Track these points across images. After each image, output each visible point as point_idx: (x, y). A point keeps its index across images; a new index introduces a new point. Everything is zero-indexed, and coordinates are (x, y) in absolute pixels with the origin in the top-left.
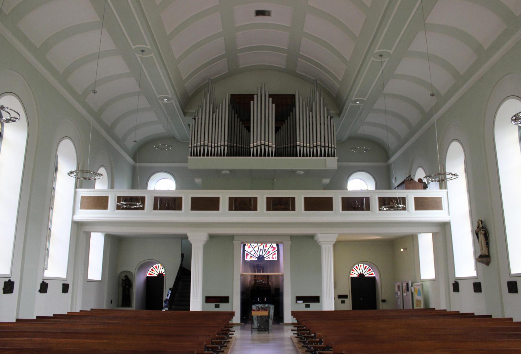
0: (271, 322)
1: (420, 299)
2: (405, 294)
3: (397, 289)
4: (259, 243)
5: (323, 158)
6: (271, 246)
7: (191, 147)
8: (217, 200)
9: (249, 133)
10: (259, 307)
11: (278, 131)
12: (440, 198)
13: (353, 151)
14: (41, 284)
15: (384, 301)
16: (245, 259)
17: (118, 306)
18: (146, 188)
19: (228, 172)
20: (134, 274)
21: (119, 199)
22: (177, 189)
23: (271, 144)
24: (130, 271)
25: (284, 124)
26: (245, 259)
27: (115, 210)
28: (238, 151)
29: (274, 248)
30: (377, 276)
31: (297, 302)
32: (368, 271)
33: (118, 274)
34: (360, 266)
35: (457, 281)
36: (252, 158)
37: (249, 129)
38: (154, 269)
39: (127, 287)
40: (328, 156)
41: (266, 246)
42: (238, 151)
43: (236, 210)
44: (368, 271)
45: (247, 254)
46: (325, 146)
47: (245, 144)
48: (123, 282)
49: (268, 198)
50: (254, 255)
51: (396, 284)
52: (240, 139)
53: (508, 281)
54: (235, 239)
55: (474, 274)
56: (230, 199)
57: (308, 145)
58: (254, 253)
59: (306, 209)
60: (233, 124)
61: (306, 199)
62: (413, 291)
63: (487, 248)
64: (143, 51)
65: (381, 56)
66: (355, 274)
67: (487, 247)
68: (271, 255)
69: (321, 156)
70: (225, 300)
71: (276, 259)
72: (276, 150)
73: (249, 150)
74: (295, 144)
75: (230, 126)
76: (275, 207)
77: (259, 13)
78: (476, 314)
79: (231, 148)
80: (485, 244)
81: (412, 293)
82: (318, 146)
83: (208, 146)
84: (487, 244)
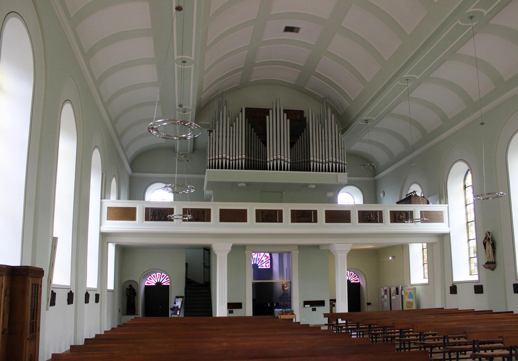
1: (412, 301)
2: (393, 298)
3: (383, 293)
5: (334, 173)
6: (265, 255)
7: (210, 160)
8: (244, 212)
9: (265, 147)
10: (283, 311)
11: (293, 146)
12: (442, 212)
13: (362, 167)
14: (86, 294)
15: (369, 304)
18: (144, 199)
19: (245, 185)
21: (185, 211)
23: (286, 158)
24: (135, 280)
25: (298, 140)
27: (144, 221)
28: (303, 166)
29: (268, 257)
30: (362, 282)
31: (304, 306)
33: (123, 283)
35: (454, 284)
36: (268, 171)
37: (265, 143)
38: (152, 278)
39: (132, 296)
40: (339, 172)
41: (260, 255)
42: (303, 166)
43: (262, 222)
47: (262, 158)
48: (128, 291)
49: (292, 211)
51: (382, 289)
52: (257, 153)
53: (514, 283)
54: (246, 249)
55: (475, 278)
56: (257, 211)
57: (321, 160)
59: (327, 222)
60: (250, 138)
61: (327, 212)
62: (403, 294)
63: (494, 256)
64: (184, 62)
65: (184, 62)
66: (153, 282)
67: (494, 255)
68: (265, 263)
69: (332, 171)
70: (239, 306)
71: (269, 267)
72: (291, 164)
73: (266, 164)
75: (247, 140)
76: (299, 219)
77: (289, 29)
78: (494, 311)
79: (248, 161)
80: (492, 252)
81: (402, 296)
82: (330, 162)
84: (494, 252)
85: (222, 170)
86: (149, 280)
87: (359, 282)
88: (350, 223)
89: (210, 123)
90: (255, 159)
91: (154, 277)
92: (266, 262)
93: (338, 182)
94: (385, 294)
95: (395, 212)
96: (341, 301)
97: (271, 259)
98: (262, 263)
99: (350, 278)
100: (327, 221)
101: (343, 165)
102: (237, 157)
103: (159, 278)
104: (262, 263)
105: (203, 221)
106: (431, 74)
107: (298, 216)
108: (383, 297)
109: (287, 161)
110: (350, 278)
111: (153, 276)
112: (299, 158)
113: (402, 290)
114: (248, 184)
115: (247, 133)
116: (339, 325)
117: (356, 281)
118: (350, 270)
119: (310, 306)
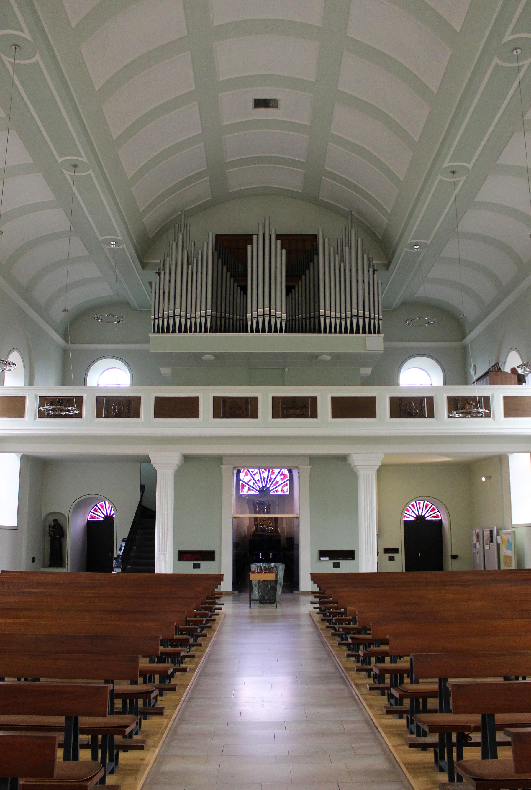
0: (279, 589)
1: (511, 555)
2: (487, 547)
4: (262, 469)
5: (361, 335)
6: (281, 472)
9: (245, 296)
10: (261, 567)
11: (291, 292)
13: (409, 324)
15: (454, 557)
16: (240, 493)
17: (44, 567)
18: (85, 383)
20: (67, 517)
21: (42, 401)
22: (132, 384)
25: (300, 282)
26: (240, 493)
28: (294, 325)
29: (285, 476)
30: (444, 519)
31: (320, 559)
32: (431, 511)
33: (44, 515)
34: (418, 504)
36: (249, 335)
37: (244, 289)
40: (370, 332)
41: (273, 473)
43: (224, 417)
44: (431, 511)
45: (243, 486)
46: (364, 317)
48: (51, 529)
49: (274, 399)
50: (254, 487)
58: (254, 484)
59: (334, 416)
61: (335, 400)
64: (75, 166)
68: (281, 486)
69: (358, 332)
70: (209, 556)
71: (288, 493)
73: (245, 322)
74: (317, 313)
76: (285, 411)
77: (260, 103)
81: (498, 545)
83: (181, 317)
85: (263, 334)
86: (94, 512)
87: (440, 520)
88: (375, 417)
89: (160, 261)
90: (227, 315)
91: (102, 507)
92: (283, 484)
93: (367, 350)
94: (477, 541)
95: (457, 398)
96: (365, 552)
97: (291, 480)
98: (277, 485)
99: (424, 512)
100: (158, 415)
101: (376, 322)
102: (198, 314)
103: (109, 509)
104: (277, 485)
105: (128, 416)
106: (496, 161)
107: (284, 406)
108: (475, 546)
109: (280, 316)
110: (424, 512)
111: (101, 505)
112: (297, 311)
113: (498, 534)
114: (219, 357)
115: (215, 274)
116: (216, 596)
117: (434, 517)
118: (415, 500)
119: (329, 560)
